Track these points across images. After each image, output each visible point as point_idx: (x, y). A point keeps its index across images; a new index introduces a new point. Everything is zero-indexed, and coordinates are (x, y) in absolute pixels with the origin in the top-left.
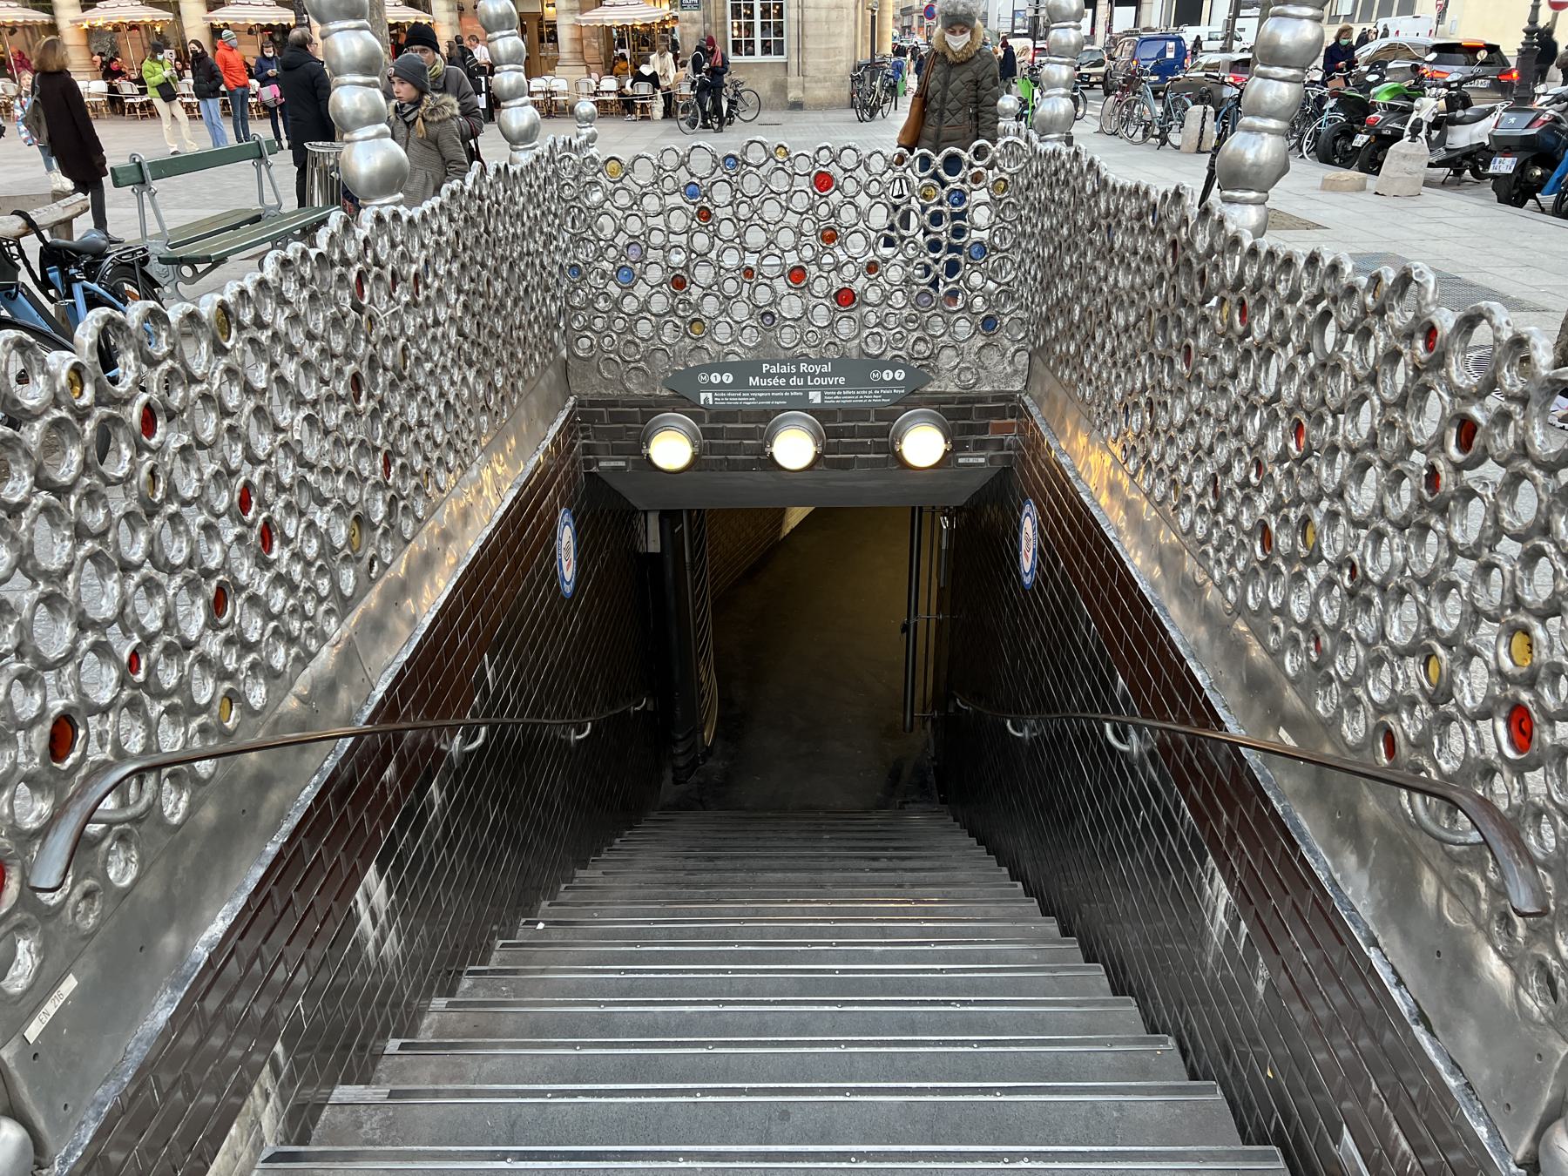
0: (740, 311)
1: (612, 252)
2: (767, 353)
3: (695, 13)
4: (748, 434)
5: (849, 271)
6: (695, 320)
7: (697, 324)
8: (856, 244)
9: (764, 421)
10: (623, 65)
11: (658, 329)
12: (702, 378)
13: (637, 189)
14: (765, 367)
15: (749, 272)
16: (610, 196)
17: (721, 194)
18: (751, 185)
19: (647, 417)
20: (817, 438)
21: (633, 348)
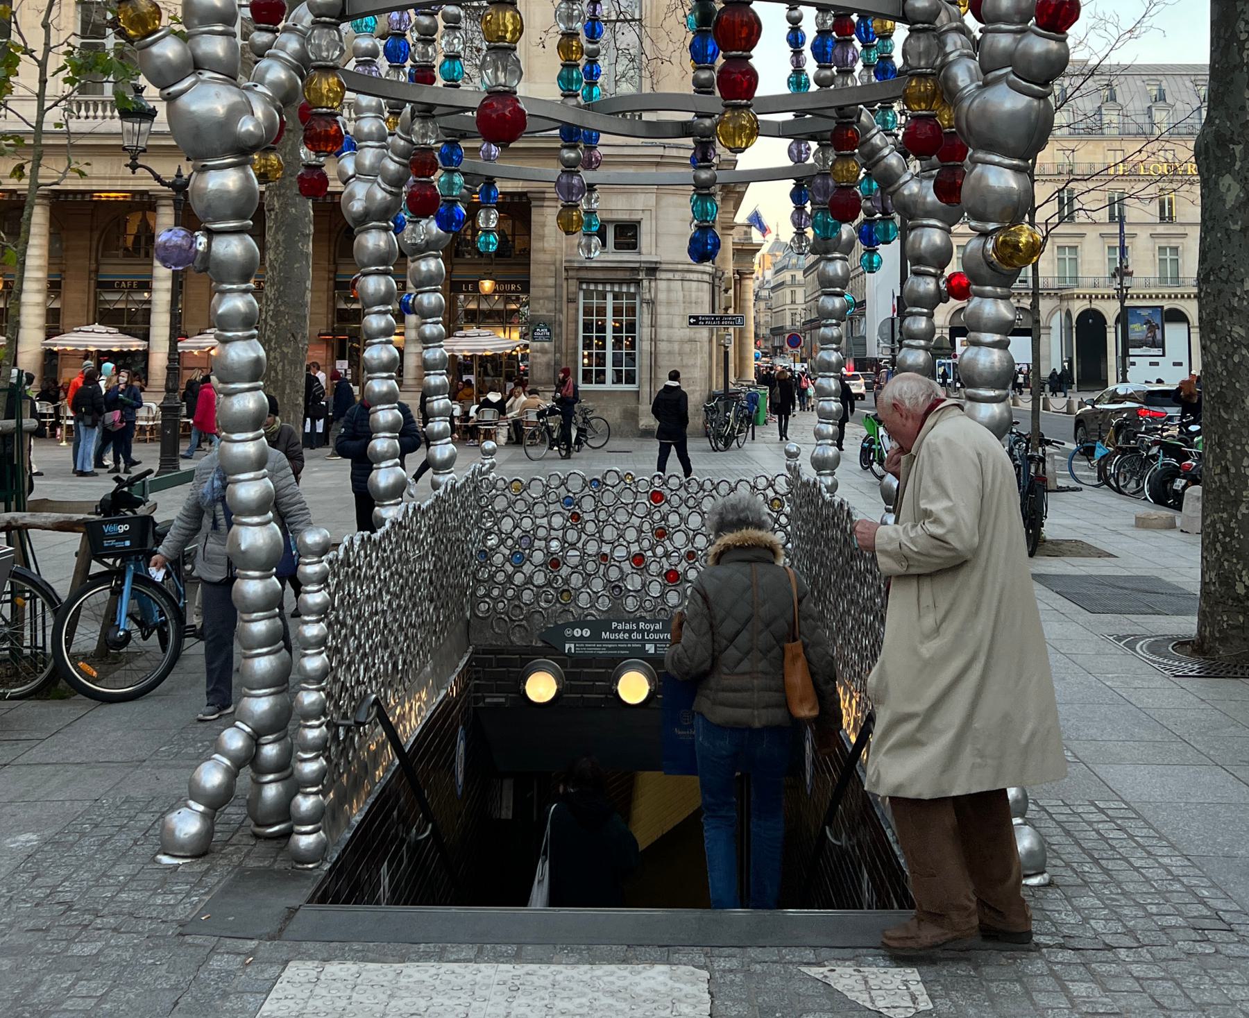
0: (597, 585)
1: (510, 542)
2: (617, 613)
3: (546, 344)
4: (599, 677)
5: (674, 560)
6: (564, 591)
7: (567, 593)
8: (679, 539)
9: (613, 667)
10: (467, 391)
11: (537, 596)
12: (568, 632)
13: (531, 500)
14: (614, 625)
15: (604, 557)
16: (511, 504)
17: (588, 504)
18: (608, 499)
19: (524, 662)
20: (651, 680)
21: (518, 611)
